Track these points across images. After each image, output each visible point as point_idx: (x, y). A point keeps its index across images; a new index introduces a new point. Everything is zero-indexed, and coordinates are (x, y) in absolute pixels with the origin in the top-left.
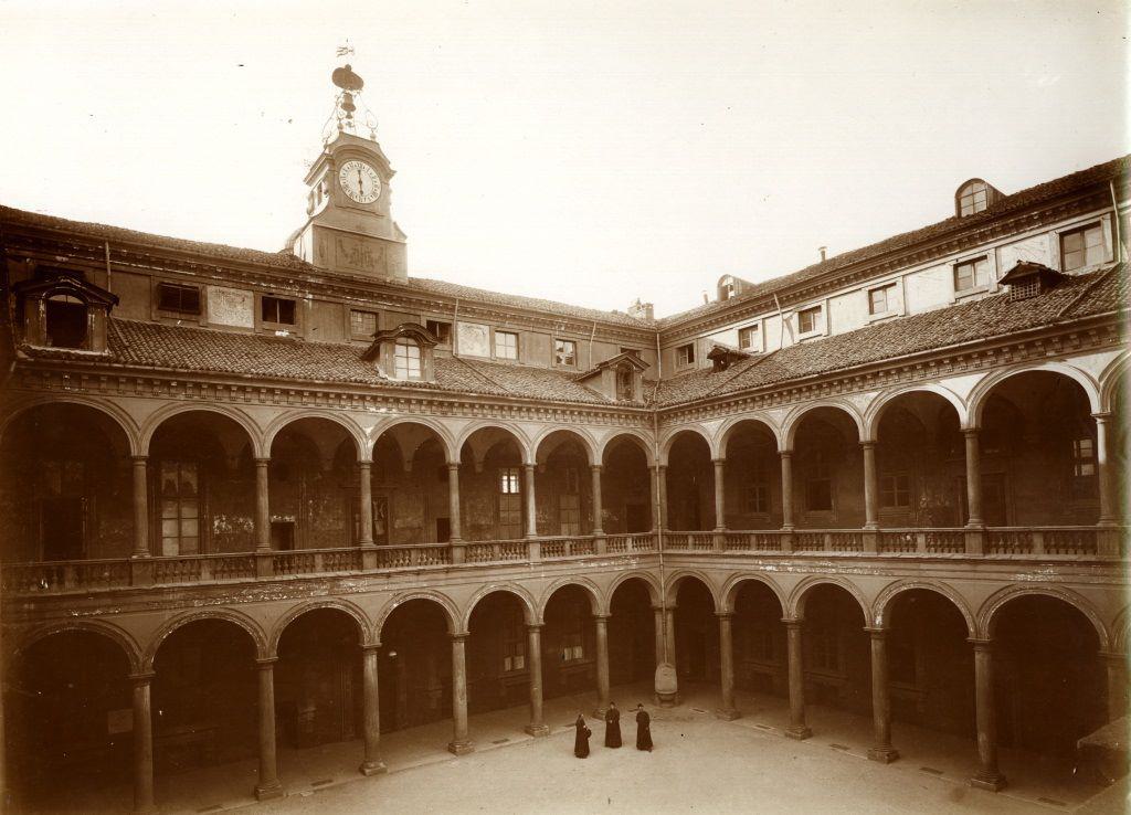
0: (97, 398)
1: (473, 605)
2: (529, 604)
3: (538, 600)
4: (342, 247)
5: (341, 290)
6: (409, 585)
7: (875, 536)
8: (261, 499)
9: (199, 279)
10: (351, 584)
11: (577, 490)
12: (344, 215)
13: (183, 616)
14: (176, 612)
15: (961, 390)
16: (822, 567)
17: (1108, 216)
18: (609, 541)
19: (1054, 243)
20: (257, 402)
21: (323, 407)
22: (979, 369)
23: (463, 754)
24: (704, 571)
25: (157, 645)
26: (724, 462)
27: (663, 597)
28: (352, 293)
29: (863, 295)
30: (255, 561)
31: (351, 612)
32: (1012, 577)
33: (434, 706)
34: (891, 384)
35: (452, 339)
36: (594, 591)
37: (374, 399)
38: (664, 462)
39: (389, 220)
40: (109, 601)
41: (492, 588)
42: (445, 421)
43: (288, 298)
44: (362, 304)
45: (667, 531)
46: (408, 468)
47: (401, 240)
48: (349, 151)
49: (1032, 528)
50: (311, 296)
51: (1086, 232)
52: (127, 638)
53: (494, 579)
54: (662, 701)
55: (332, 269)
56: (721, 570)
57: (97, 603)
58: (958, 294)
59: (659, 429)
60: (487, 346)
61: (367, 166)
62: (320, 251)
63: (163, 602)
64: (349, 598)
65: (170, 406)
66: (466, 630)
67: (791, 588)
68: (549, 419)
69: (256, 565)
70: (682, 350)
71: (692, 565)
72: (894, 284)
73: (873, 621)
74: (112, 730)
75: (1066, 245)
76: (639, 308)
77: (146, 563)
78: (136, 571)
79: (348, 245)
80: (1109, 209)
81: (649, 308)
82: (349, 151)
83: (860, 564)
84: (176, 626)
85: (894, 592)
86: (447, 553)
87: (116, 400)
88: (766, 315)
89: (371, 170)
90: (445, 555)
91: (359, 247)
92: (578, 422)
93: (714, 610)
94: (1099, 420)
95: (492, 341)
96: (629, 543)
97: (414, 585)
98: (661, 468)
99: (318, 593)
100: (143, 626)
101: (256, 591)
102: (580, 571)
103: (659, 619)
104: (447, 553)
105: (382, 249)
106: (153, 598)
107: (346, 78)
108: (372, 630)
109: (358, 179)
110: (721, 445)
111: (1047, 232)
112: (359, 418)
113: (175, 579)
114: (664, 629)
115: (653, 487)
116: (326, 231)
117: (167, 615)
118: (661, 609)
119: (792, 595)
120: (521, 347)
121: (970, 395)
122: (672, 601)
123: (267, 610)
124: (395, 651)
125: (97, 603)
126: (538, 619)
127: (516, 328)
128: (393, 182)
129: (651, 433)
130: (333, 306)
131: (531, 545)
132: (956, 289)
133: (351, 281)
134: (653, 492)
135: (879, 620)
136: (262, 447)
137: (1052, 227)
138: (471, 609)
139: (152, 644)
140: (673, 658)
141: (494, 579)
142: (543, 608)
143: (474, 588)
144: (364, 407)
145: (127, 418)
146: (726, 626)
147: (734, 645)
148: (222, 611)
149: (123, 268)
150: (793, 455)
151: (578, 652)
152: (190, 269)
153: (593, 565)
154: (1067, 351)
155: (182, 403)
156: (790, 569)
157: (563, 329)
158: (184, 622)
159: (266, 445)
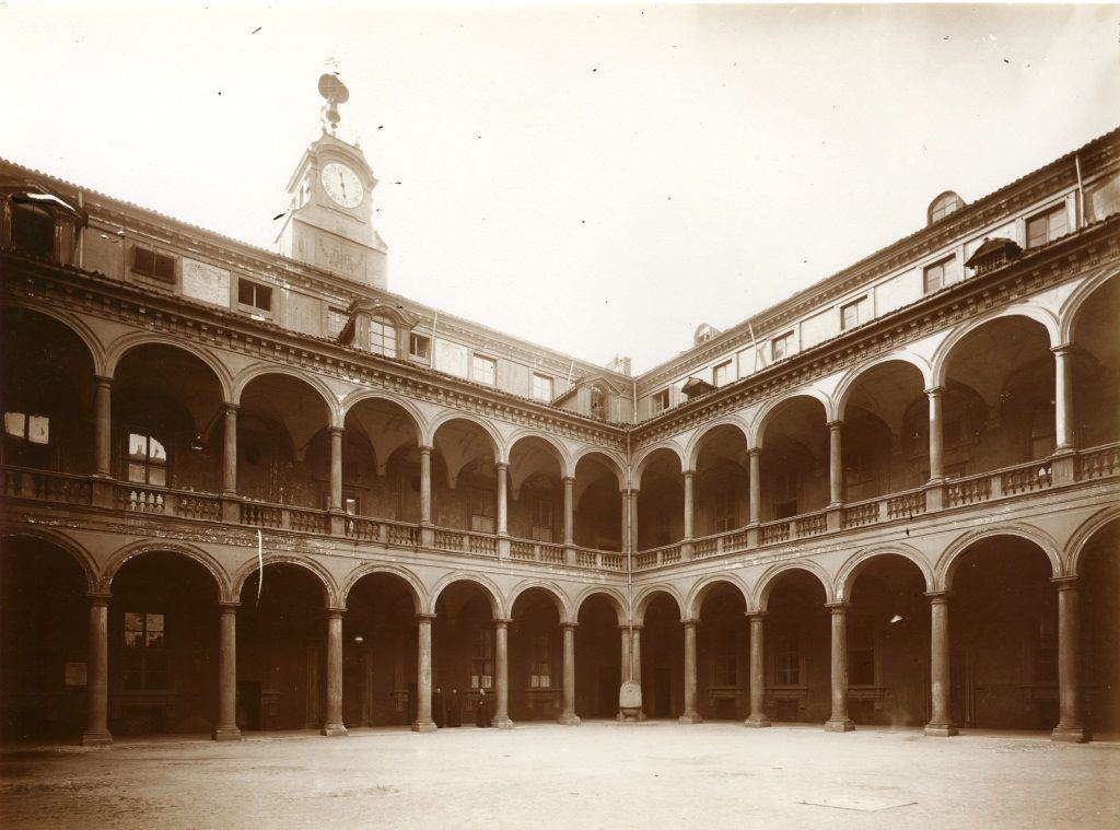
0: (63, 312)
1: (441, 589)
2: (497, 598)
3: (506, 596)
4: (321, 245)
5: (321, 285)
6: (377, 557)
7: (838, 513)
8: (231, 428)
9: (176, 250)
10: (318, 545)
11: (550, 524)
12: (325, 215)
13: (144, 543)
14: (138, 539)
15: (925, 353)
16: (786, 553)
17: (1073, 194)
18: (579, 553)
19: (1020, 229)
20: (228, 347)
21: (296, 365)
22: (944, 327)
23: (425, 732)
24: (670, 582)
25: (116, 568)
26: (693, 474)
27: (631, 616)
28: (330, 289)
29: (837, 310)
30: (221, 505)
31: (316, 572)
32: (970, 523)
33: (400, 708)
34: (858, 360)
35: (429, 354)
36: (562, 597)
37: (348, 367)
38: (636, 485)
39: (370, 228)
40: (66, 514)
41: (461, 576)
42: (419, 404)
43: (265, 284)
44: (340, 303)
45: (636, 552)
46: (381, 472)
47: (382, 249)
48: (331, 151)
49: (991, 473)
50: (288, 286)
51: (1051, 216)
52: (85, 554)
53: (464, 567)
54: (626, 716)
55: (311, 262)
56: (686, 580)
57: (53, 514)
58: (926, 295)
59: (632, 453)
60: (465, 368)
61: (350, 171)
62: (300, 247)
63: (123, 525)
64: (317, 558)
65: (139, 334)
66: (432, 611)
67: (754, 583)
68: (523, 423)
69: (221, 509)
70: (657, 397)
71: (660, 579)
72: (866, 297)
73: (834, 596)
74: (69, 681)
75: (1032, 232)
76: (617, 363)
77: (107, 484)
78: (96, 491)
79: (329, 244)
80: (1074, 187)
81: (627, 361)
82: (331, 151)
83: (822, 543)
84: (137, 552)
85: (856, 563)
86: (417, 536)
87: (82, 317)
88: (741, 348)
89: (354, 176)
90: (414, 536)
91: (339, 249)
92: (552, 431)
93: (680, 618)
94: (1057, 354)
95: (470, 363)
96: (599, 559)
97: (382, 558)
98: (633, 491)
99: (284, 547)
100: (107, 547)
101: (220, 533)
102: (548, 576)
103: (625, 637)
104: (417, 536)
105: (362, 255)
106: (111, 520)
107: (332, 88)
108: (338, 593)
109: (339, 182)
110: (692, 457)
111: (1014, 220)
112: (332, 384)
113: (141, 507)
114: (631, 651)
115: (624, 509)
116: (307, 227)
117: (128, 540)
118: (627, 628)
119: (754, 593)
120: (499, 373)
121: (934, 356)
122: (639, 621)
123: (235, 557)
124: (363, 637)
125: (53, 514)
126: (506, 615)
127: (492, 354)
128: (376, 193)
129: (623, 455)
130: (311, 301)
131: (501, 542)
132: (925, 291)
133: (330, 276)
134: (624, 515)
135: (840, 594)
136: (231, 392)
137: (1019, 214)
138: (438, 592)
139: (111, 565)
140: (639, 677)
141: (464, 567)
142: (511, 605)
143: (441, 572)
144: (338, 374)
145: (96, 341)
146: (690, 633)
147: (699, 677)
148: (186, 546)
149: (97, 224)
150: (765, 618)
151: (545, 683)
152: (166, 237)
153: (562, 572)
154: (1029, 291)
155: (151, 333)
156: (755, 562)
157: (540, 363)
158: (146, 550)
159: (236, 393)
